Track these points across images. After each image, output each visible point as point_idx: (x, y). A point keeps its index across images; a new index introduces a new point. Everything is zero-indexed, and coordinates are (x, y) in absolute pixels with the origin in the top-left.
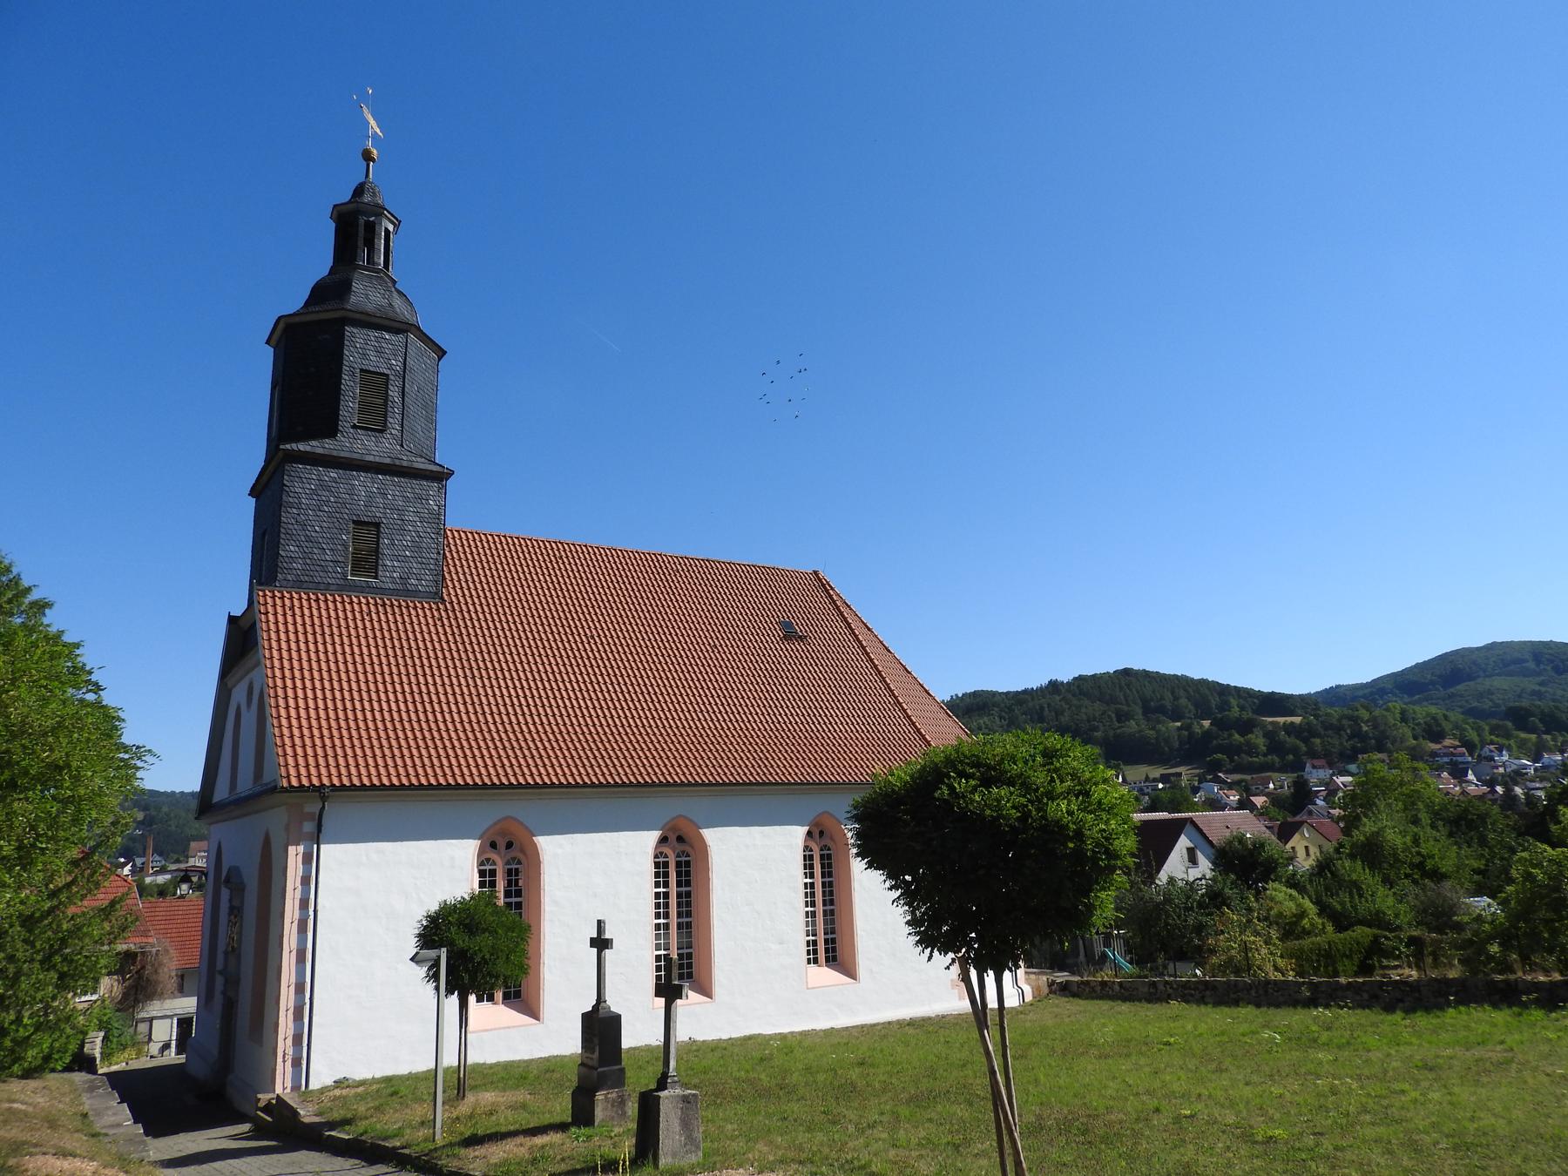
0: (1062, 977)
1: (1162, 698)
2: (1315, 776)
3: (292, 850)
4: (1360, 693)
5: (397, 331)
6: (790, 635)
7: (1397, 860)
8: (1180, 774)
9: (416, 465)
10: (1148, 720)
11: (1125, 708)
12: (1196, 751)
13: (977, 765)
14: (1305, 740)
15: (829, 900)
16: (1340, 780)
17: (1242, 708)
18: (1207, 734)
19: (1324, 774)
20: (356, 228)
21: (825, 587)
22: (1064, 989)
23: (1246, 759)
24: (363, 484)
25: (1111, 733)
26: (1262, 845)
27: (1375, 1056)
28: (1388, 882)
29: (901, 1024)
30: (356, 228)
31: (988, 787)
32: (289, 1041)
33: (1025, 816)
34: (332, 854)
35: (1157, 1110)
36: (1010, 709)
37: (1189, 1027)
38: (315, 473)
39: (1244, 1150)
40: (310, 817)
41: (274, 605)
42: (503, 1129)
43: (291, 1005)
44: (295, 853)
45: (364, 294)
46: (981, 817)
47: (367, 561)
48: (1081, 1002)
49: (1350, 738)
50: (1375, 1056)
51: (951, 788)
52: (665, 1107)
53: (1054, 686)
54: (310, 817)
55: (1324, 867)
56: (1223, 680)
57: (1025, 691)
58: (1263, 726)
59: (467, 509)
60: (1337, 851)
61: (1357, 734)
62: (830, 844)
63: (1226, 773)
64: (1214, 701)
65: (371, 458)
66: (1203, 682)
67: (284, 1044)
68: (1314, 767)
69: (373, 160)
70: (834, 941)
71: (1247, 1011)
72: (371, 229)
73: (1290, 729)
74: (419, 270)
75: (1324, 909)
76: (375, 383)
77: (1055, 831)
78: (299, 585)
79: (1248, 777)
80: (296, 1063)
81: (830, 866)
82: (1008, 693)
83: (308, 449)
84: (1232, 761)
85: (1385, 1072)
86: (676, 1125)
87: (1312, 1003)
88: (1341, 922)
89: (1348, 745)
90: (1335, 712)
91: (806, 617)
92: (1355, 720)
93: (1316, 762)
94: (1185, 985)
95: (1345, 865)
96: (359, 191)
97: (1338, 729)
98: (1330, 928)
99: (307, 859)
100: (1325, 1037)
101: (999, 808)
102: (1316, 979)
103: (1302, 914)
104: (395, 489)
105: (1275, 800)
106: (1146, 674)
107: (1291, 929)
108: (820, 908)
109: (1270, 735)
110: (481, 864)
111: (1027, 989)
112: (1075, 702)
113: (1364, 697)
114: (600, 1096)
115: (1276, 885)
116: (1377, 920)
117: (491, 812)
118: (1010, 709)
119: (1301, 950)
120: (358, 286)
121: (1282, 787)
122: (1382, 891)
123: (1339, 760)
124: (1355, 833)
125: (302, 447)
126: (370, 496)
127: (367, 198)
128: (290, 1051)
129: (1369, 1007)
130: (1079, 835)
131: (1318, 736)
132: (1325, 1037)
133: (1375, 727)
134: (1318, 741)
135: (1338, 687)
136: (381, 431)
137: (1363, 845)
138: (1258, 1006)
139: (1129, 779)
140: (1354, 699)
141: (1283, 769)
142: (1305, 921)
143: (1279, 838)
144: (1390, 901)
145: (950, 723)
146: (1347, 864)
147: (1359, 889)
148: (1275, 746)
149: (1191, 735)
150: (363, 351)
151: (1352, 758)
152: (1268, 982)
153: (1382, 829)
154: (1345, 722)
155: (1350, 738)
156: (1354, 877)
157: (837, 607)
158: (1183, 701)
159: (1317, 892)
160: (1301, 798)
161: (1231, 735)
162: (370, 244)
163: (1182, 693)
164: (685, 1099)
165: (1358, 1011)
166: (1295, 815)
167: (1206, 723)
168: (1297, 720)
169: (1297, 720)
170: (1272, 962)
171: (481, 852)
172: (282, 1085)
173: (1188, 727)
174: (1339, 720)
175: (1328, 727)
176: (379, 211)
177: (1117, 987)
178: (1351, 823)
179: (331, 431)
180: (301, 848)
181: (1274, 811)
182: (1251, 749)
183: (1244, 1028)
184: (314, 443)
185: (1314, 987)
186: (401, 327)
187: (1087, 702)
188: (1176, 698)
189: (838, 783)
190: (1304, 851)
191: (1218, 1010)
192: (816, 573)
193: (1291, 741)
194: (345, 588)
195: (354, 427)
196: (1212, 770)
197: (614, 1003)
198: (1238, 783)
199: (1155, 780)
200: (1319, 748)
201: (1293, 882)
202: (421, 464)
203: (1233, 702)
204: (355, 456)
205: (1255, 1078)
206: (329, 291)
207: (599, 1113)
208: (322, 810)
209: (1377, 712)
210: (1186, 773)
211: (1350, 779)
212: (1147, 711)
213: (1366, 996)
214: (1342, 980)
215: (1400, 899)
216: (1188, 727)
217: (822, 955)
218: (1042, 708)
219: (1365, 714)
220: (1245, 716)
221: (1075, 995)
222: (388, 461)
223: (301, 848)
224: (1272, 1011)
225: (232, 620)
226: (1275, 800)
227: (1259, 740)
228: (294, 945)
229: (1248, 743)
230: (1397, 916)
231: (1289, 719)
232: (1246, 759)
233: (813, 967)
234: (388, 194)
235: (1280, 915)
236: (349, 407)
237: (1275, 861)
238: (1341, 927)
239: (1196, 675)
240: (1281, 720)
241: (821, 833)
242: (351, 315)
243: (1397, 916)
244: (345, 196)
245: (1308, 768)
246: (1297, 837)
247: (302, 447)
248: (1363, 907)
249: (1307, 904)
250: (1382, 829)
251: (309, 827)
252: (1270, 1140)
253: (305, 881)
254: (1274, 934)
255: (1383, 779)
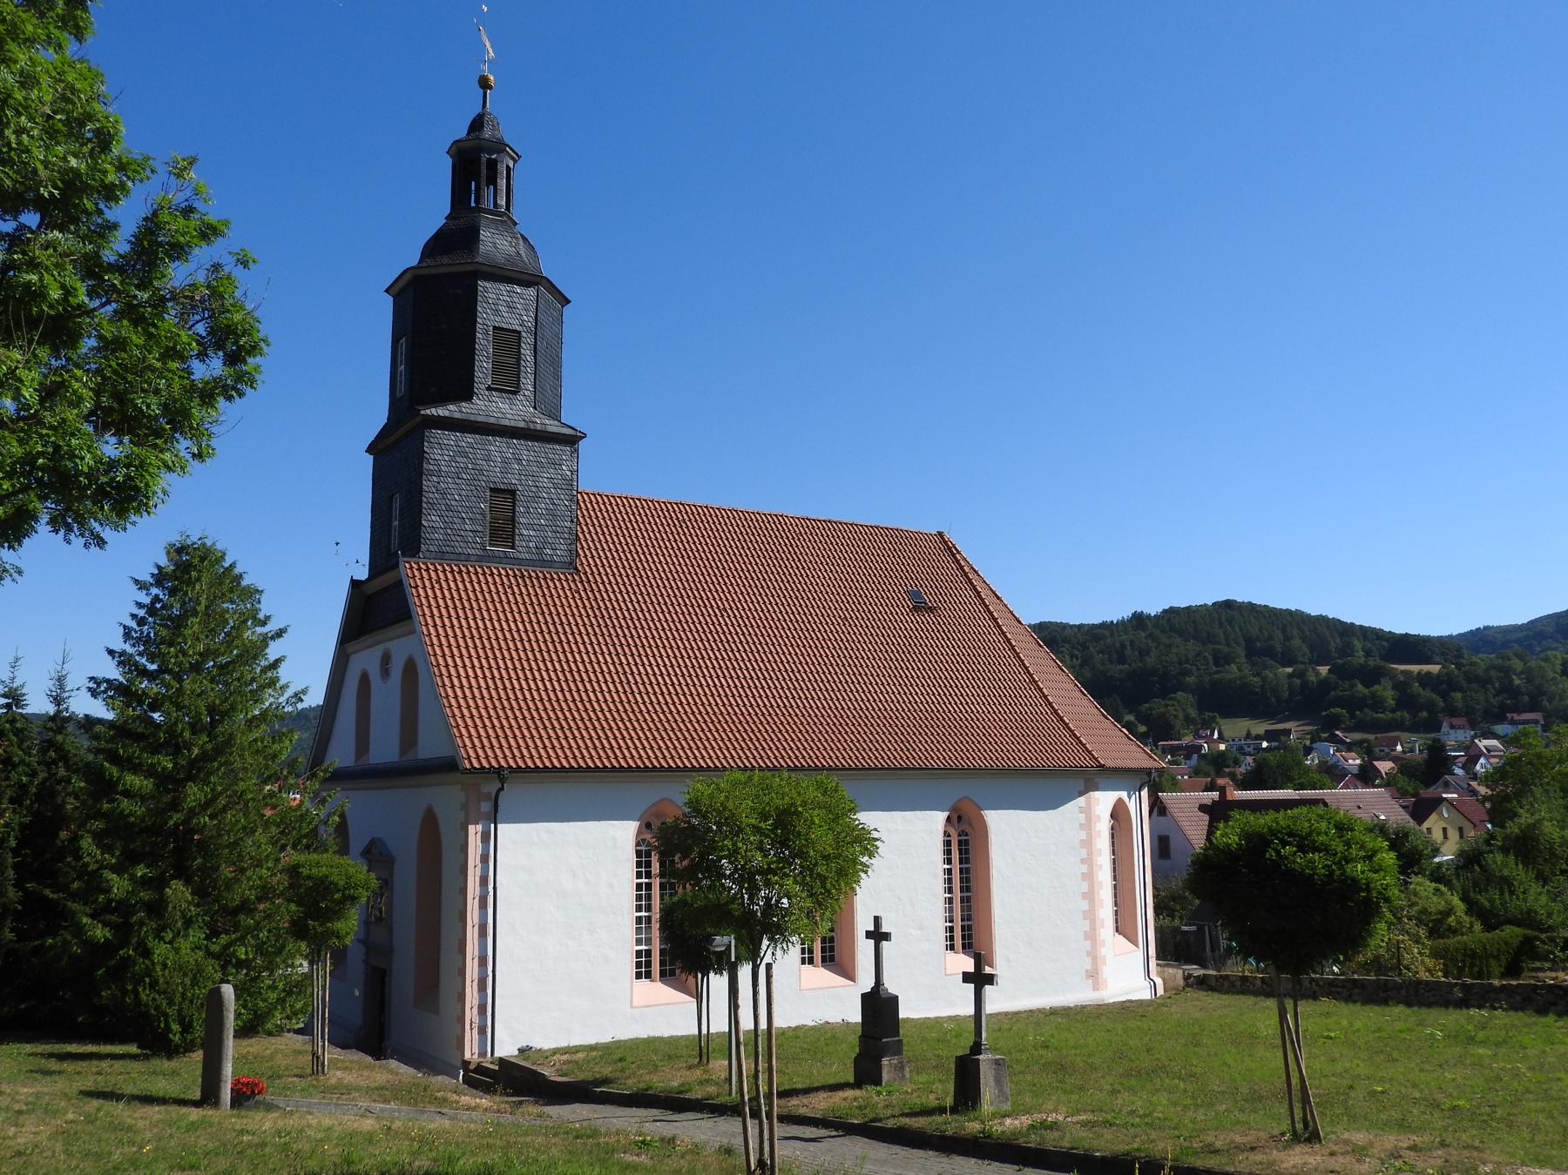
0: (1197, 971)
1: (1270, 638)
2: (1454, 737)
3: (471, 828)
4: (1513, 637)
5: (526, 284)
6: (919, 607)
7: (1553, 855)
8: (1288, 732)
9: (550, 429)
10: (1253, 664)
11: (1226, 650)
12: (1311, 704)
13: (1291, 834)
14: (1444, 695)
15: (965, 888)
16: (1483, 744)
17: (1368, 653)
18: (1324, 684)
19: (1463, 735)
20: (476, 163)
21: (951, 550)
22: (1202, 983)
23: (1370, 714)
24: (496, 446)
25: (1207, 679)
26: (1406, 835)
27: (1531, 1052)
28: (1543, 879)
29: (1053, 1012)
30: (476, 163)
31: (1305, 852)
32: (475, 1011)
33: (1332, 873)
34: (507, 832)
35: (1351, 1087)
36: (1084, 646)
37: (1345, 1023)
38: (450, 438)
39: (1437, 1114)
40: (487, 797)
41: (422, 578)
42: (799, 1086)
43: (476, 976)
44: (474, 831)
45: (493, 243)
46: (1302, 874)
47: (503, 529)
48: (1224, 997)
49: (1498, 693)
50: (1531, 1052)
51: (1278, 852)
52: (983, 1068)
53: (1139, 619)
54: (487, 797)
55: (1470, 859)
56: (1347, 618)
57: (1103, 625)
58: (1392, 675)
59: (601, 471)
60: (1488, 842)
61: (1508, 689)
62: (969, 830)
63: (1344, 730)
64: (1334, 643)
65: (506, 423)
66: (1322, 620)
67: (471, 1014)
68: (1452, 727)
69: (490, 87)
70: (970, 928)
71: (1399, 1010)
72: (492, 165)
73: (1425, 679)
74: (541, 216)
75: (1472, 908)
76: (507, 340)
77: (1352, 885)
78: (441, 556)
79: (1371, 737)
80: (482, 1030)
81: (967, 851)
82: (1081, 626)
83: (447, 413)
84: (1353, 716)
85: (1542, 1065)
86: (992, 1082)
87: (1463, 1004)
88: (1490, 920)
89: (1495, 701)
90: (1482, 660)
91: (930, 580)
92: (1506, 671)
93: (1456, 721)
94: (1332, 983)
95: (1496, 860)
96: (477, 124)
97: (1484, 682)
98: (1478, 927)
99: (485, 837)
100: (1481, 1035)
101: (1314, 868)
102: (1469, 981)
103: (1449, 912)
104: (527, 451)
105: (1405, 768)
106: (1252, 608)
107: (1437, 926)
108: (957, 894)
109: (1402, 686)
110: (638, 844)
111: (1159, 981)
112: (1164, 639)
113: (1518, 641)
114: (885, 1061)
115: (1419, 879)
116: (1528, 919)
117: (956, 790)
118: (1084, 646)
119: (1446, 950)
120: (485, 234)
121: (1412, 750)
122: (1535, 888)
123: (1483, 722)
124: (1509, 824)
125: (441, 412)
126: (505, 461)
127: (487, 133)
128: (476, 1019)
129: (1523, 1009)
130: (1368, 889)
131: (1461, 690)
132: (1481, 1035)
133: (1529, 680)
134: (1458, 695)
135: (1486, 628)
136: (514, 393)
137: (1517, 838)
138: (1409, 1005)
139: (1226, 734)
140: (1506, 644)
141: (1414, 728)
142: (1452, 919)
143: (1413, 816)
144: (1544, 899)
145: (1085, 702)
146: (1499, 858)
147: (1510, 885)
148: (1406, 700)
149: (1305, 684)
150: (499, 307)
151: (1500, 718)
152: (1419, 982)
153: (1539, 821)
154: (1493, 673)
155: (1498, 693)
156: (1506, 872)
157: (966, 574)
158: (1296, 642)
159: (1463, 888)
160: (1435, 766)
161: (1353, 686)
162: (492, 180)
163: (1295, 632)
164: (997, 1062)
165: (1512, 1013)
166: (1428, 786)
167: (1324, 670)
168: (1435, 669)
169: (1435, 669)
170: (1421, 964)
171: (639, 833)
172: (471, 1052)
173: (1300, 675)
174: (1486, 671)
175: (1472, 678)
176: (500, 146)
177: (1258, 982)
178: (1500, 811)
179: (467, 394)
180: (479, 827)
181: (1403, 781)
182: (1377, 704)
183: (1400, 1025)
184: (452, 407)
185: (1466, 988)
186: (531, 279)
187: (1178, 640)
188: (1287, 639)
189: (981, 769)
190: (1445, 839)
191: (1367, 1008)
192: (940, 534)
193: (1426, 694)
194: (485, 558)
195: (489, 389)
196: (1327, 728)
197: (891, 985)
198: (1359, 743)
199: (1259, 738)
200: (1460, 705)
201: (1437, 876)
202: (552, 427)
203: (1358, 644)
204: (492, 420)
205: (1427, 1067)
206: (456, 237)
207: (885, 1076)
208: (498, 790)
209: (1533, 664)
210: (1296, 730)
211: (1494, 742)
212: (1251, 653)
213: (1518, 998)
214: (1496, 982)
215: (1554, 897)
216: (1300, 675)
217: (958, 942)
218: (1123, 646)
219: (1518, 665)
220: (1371, 663)
221: (1212, 989)
222: (522, 425)
223: (479, 827)
224: (1424, 1011)
225: (355, 584)
226: (1405, 768)
227: (1387, 692)
228: (476, 921)
229: (1373, 696)
230: (1550, 915)
231: (1426, 668)
232: (1370, 714)
233: (644, 982)
234: (507, 128)
235: (1424, 911)
236: (483, 367)
237: (1420, 854)
238: (1489, 927)
239: (1314, 611)
240: (1415, 668)
241: (960, 818)
242: (485, 269)
243: (1550, 915)
244: (462, 133)
245: (1445, 727)
246: (1434, 816)
247: (441, 412)
248: (1515, 905)
249: (1456, 901)
250: (1539, 821)
251: (486, 807)
252: (1454, 1108)
253: (484, 859)
254: (1422, 932)
255: (1539, 756)
